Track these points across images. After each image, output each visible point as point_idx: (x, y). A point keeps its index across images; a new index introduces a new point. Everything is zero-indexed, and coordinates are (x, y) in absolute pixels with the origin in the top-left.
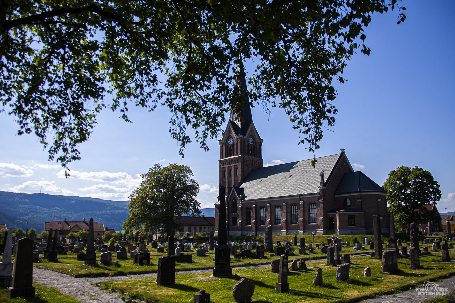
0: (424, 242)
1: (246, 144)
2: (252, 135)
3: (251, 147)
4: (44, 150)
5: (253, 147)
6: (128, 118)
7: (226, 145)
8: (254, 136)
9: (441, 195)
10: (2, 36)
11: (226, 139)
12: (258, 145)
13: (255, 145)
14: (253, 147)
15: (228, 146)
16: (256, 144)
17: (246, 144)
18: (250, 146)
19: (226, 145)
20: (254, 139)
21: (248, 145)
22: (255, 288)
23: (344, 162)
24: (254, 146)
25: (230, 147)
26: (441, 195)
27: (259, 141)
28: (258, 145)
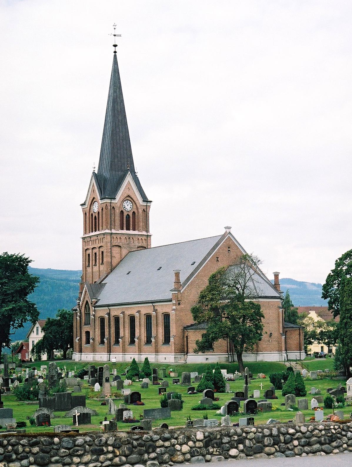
7: (91, 213)
12: (140, 211)
13: (136, 211)
15: (92, 214)
16: (137, 208)
17: (118, 212)
18: (125, 214)
19: (91, 213)
20: (133, 201)
21: (122, 212)
23: (229, 248)
24: (134, 212)
25: (95, 217)
27: (145, 204)
28: (140, 211)
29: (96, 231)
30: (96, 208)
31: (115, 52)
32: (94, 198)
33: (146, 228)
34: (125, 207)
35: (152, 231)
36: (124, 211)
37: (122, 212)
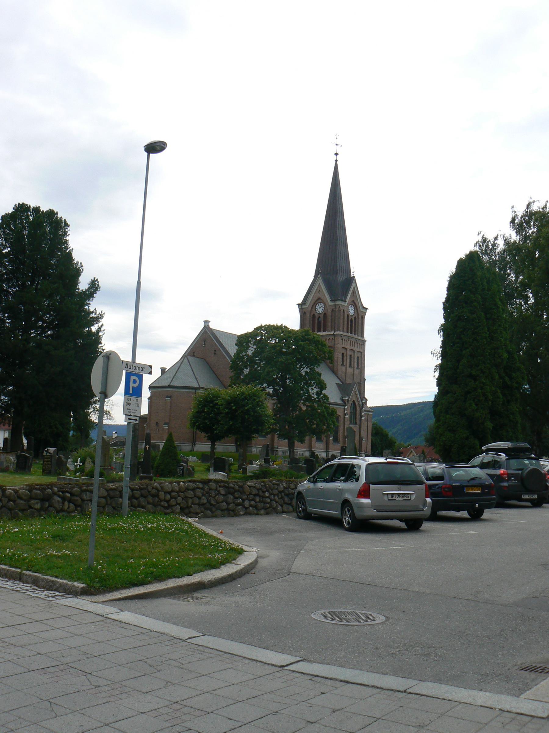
1: (346, 315)
2: (353, 301)
3: (351, 320)
8: (357, 303)
17: (346, 315)
19: (312, 314)
21: (348, 315)
24: (355, 317)
28: (360, 317)
30: (320, 309)
31: (336, 161)
32: (319, 299)
34: (322, 310)
36: (350, 316)
37: (348, 315)
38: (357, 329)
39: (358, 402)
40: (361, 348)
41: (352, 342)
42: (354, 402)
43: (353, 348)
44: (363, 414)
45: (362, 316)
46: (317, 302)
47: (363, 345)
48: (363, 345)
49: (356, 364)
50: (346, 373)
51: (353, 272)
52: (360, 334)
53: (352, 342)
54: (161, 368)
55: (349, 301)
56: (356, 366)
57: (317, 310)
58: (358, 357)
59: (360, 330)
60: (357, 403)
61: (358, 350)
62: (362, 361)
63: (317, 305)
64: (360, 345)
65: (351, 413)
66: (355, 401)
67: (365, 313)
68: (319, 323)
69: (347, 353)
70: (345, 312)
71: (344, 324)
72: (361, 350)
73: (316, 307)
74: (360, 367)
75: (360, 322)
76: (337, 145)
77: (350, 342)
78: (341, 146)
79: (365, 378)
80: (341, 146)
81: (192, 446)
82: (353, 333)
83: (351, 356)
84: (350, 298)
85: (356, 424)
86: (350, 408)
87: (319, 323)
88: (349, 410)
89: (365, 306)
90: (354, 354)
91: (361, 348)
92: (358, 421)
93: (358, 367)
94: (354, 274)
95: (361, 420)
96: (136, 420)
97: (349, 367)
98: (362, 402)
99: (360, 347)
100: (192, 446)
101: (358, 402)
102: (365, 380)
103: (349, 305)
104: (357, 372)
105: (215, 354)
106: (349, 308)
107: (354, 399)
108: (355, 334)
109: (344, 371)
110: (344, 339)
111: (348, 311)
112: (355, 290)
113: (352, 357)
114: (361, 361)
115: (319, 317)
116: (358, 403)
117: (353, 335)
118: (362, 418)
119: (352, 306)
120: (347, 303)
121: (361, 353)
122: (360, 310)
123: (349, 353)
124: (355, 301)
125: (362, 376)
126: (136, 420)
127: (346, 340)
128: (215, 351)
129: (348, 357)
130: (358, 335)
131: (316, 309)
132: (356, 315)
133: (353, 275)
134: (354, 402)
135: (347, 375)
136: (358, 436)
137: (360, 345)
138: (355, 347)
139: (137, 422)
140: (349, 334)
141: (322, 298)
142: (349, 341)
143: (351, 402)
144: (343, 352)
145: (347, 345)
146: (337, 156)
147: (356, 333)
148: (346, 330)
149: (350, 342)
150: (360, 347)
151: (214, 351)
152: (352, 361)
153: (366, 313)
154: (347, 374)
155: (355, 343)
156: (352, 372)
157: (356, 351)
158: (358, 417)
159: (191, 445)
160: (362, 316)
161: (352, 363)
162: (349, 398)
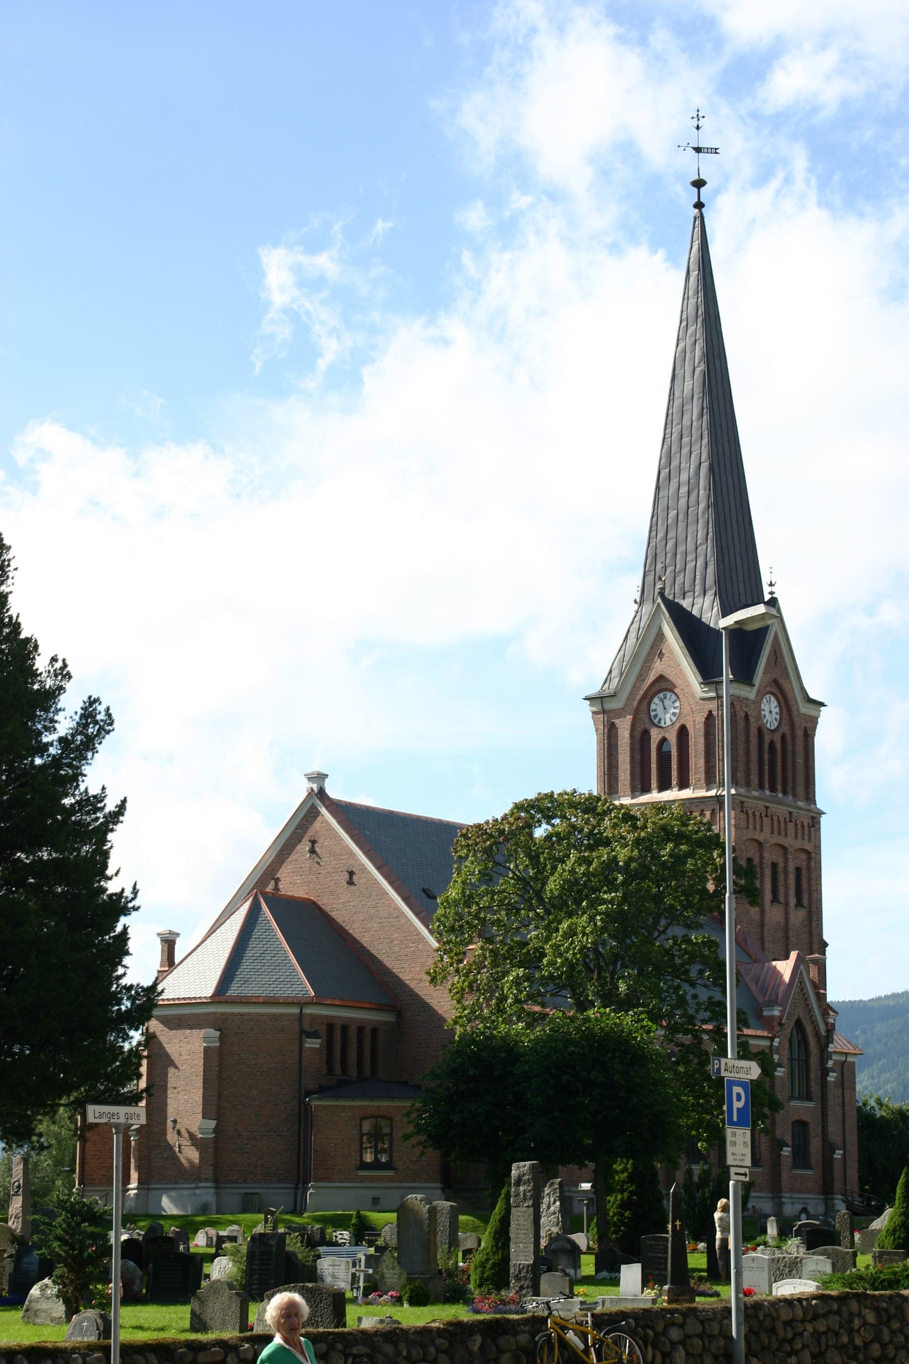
0: (714, 876)
1: (754, 730)
2: (775, 681)
3: (772, 745)
4: (14, 557)
5: (778, 745)
6: (836, 1022)
8: (786, 687)
9: (121, 801)
10: (124, 1086)
11: (792, 703)
12: (800, 733)
14: (778, 745)
17: (754, 730)
18: (767, 739)
21: (760, 731)
22: (729, 1138)
24: (783, 737)
26: (121, 801)
28: (800, 733)
29: (664, 786)
33: (810, 796)
35: (820, 804)
36: (766, 731)
37: (760, 731)
38: (790, 775)
39: (813, 1022)
40: (806, 837)
41: (779, 821)
42: (799, 1023)
43: (781, 840)
44: (830, 1063)
45: (806, 730)
46: (655, 689)
47: (813, 826)
48: (813, 826)
49: (792, 892)
50: (762, 925)
51: (771, 585)
52: (800, 789)
53: (779, 821)
54: (158, 934)
55: (761, 681)
56: (793, 901)
57: (656, 716)
58: (798, 870)
59: (800, 779)
60: (809, 1029)
61: (798, 844)
62: (813, 883)
63: (656, 700)
64: (803, 826)
65: (791, 1059)
66: (803, 1020)
67: (814, 721)
68: (663, 758)
69: (761, 857)
70: (752, 720)
71: (748, 761)
72: (808, 846)
73: (653, 707)
74: (805, 902)
75: (800, 749)
76: (698, 150)
77: (772, 819)
78: (715, 151)
79: (825, 938)
80: (715, 151)
81: (296, 1195)
82: (779, 787)
83: (774, 866)
84: (764, 673)
85: (809, 1098)
86: (787, 1045)
87: (663, 758)
88: (786, 1053)
89: (812, 695)
90: (786, 860)
91: (806, 837)
92: (815, 1088)
93: (799, 904)
94: (774, 589)
95: (824, 1083)
96: (745, 1175)
97: (772, 902)
98: (827, 1024)
99: (803, 833)
100: (296, 1195)
101: (813, 1022)
102: (826, 945)
103: (761, 695)
104: (798, 917)
105: (351, 883)
106: (763, 707)
107: (800, 1012)
108: (785, 792)
109: (757, 918)
110: (750, 812)
111: (759, 717)
112: (779, 646)
113: (804, 873)
114: (810, 879)
115: (664, 740)
116: (815, 1028)
117: (780, 795)
118: (829, 1079)
119: (773, 698)
120: (756, 688)
121: (808, 853)
122: (798, 710)
123: (770, 856)
124: (782, 681)
125: (815, 933)
126: (745, 1175)
127: (757, 814)
128: (351, 873)
129: (768, 873)
130: (795, 796)
131: (652, 714)
132: (786, 729)
133: (771, 593)
134: (799, 1023)
135: (766, 933)
136: (819, 1139)
137: (803, 826)
138: (786, 835)
139: (747, 1179)
140: (767, 792)
141: (671, 677)
142: (790, 821)
143: (790, 1025)
144: (749, 855)
145: (762, 830)
146: (702, 189)
147: (789, 789)
148: (757, 782)
149: (772, 819)
150: (803, 833)
151: (347, 876)
152: (781, 882)
153: (817, 718)
154: (766, 928)
155: (785, 822)
156: (782, 921)
157: (790, 850)
158: (814, 1074)
159: (293, 1191)
160: (806, 730)
161: (781, 890)
162: (782, 1012)
